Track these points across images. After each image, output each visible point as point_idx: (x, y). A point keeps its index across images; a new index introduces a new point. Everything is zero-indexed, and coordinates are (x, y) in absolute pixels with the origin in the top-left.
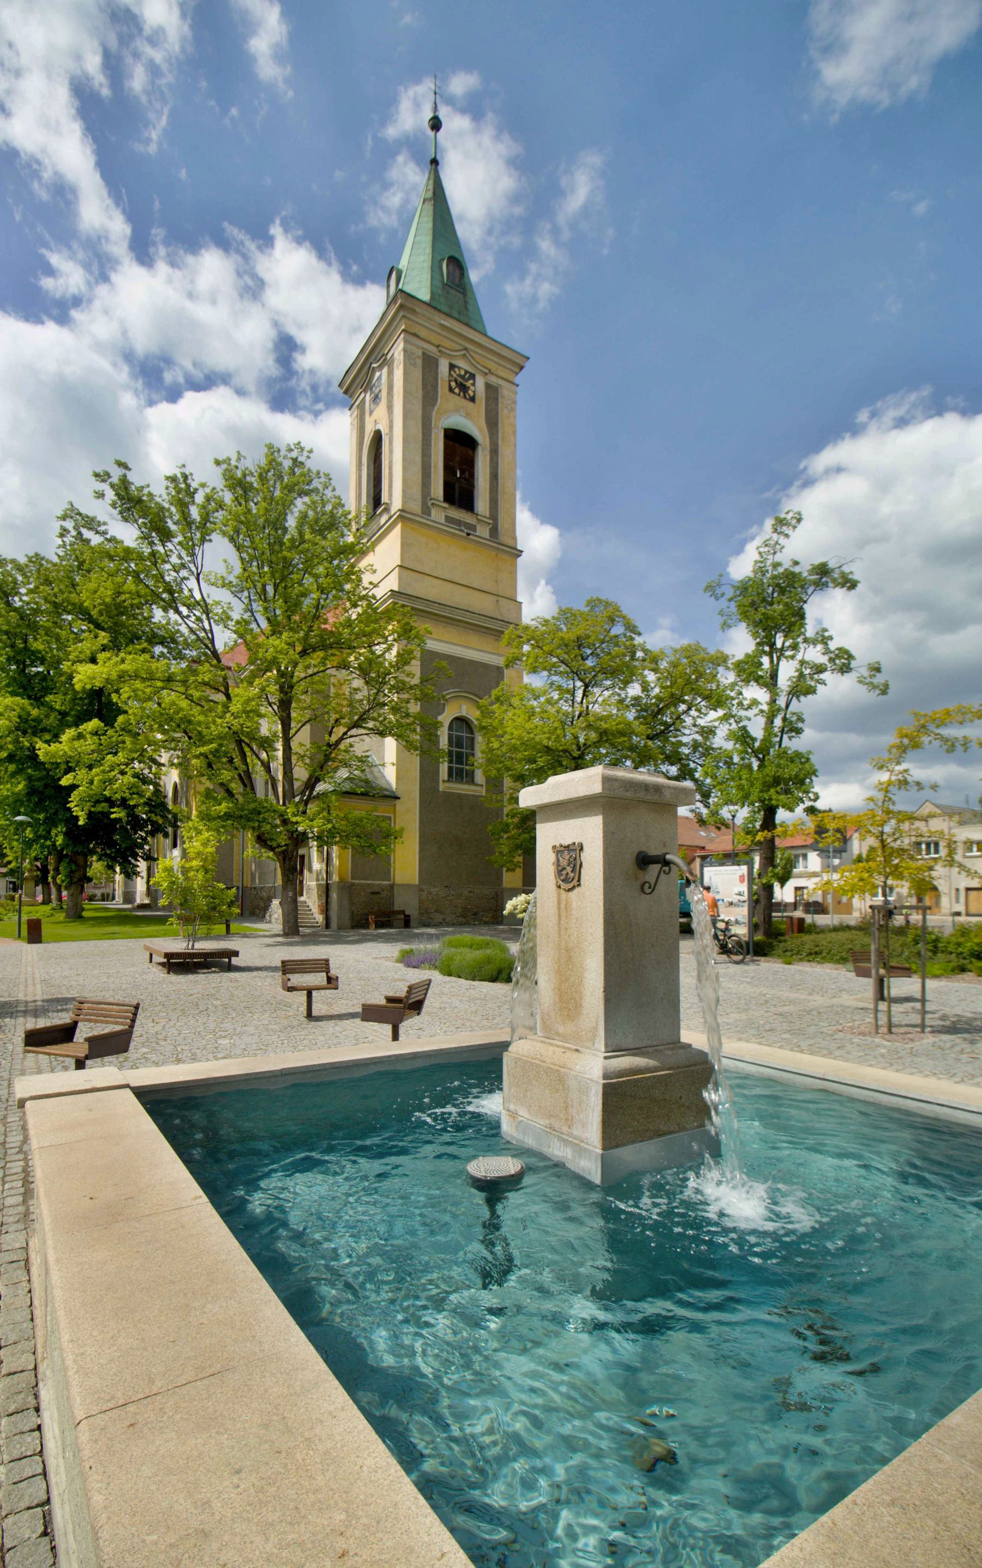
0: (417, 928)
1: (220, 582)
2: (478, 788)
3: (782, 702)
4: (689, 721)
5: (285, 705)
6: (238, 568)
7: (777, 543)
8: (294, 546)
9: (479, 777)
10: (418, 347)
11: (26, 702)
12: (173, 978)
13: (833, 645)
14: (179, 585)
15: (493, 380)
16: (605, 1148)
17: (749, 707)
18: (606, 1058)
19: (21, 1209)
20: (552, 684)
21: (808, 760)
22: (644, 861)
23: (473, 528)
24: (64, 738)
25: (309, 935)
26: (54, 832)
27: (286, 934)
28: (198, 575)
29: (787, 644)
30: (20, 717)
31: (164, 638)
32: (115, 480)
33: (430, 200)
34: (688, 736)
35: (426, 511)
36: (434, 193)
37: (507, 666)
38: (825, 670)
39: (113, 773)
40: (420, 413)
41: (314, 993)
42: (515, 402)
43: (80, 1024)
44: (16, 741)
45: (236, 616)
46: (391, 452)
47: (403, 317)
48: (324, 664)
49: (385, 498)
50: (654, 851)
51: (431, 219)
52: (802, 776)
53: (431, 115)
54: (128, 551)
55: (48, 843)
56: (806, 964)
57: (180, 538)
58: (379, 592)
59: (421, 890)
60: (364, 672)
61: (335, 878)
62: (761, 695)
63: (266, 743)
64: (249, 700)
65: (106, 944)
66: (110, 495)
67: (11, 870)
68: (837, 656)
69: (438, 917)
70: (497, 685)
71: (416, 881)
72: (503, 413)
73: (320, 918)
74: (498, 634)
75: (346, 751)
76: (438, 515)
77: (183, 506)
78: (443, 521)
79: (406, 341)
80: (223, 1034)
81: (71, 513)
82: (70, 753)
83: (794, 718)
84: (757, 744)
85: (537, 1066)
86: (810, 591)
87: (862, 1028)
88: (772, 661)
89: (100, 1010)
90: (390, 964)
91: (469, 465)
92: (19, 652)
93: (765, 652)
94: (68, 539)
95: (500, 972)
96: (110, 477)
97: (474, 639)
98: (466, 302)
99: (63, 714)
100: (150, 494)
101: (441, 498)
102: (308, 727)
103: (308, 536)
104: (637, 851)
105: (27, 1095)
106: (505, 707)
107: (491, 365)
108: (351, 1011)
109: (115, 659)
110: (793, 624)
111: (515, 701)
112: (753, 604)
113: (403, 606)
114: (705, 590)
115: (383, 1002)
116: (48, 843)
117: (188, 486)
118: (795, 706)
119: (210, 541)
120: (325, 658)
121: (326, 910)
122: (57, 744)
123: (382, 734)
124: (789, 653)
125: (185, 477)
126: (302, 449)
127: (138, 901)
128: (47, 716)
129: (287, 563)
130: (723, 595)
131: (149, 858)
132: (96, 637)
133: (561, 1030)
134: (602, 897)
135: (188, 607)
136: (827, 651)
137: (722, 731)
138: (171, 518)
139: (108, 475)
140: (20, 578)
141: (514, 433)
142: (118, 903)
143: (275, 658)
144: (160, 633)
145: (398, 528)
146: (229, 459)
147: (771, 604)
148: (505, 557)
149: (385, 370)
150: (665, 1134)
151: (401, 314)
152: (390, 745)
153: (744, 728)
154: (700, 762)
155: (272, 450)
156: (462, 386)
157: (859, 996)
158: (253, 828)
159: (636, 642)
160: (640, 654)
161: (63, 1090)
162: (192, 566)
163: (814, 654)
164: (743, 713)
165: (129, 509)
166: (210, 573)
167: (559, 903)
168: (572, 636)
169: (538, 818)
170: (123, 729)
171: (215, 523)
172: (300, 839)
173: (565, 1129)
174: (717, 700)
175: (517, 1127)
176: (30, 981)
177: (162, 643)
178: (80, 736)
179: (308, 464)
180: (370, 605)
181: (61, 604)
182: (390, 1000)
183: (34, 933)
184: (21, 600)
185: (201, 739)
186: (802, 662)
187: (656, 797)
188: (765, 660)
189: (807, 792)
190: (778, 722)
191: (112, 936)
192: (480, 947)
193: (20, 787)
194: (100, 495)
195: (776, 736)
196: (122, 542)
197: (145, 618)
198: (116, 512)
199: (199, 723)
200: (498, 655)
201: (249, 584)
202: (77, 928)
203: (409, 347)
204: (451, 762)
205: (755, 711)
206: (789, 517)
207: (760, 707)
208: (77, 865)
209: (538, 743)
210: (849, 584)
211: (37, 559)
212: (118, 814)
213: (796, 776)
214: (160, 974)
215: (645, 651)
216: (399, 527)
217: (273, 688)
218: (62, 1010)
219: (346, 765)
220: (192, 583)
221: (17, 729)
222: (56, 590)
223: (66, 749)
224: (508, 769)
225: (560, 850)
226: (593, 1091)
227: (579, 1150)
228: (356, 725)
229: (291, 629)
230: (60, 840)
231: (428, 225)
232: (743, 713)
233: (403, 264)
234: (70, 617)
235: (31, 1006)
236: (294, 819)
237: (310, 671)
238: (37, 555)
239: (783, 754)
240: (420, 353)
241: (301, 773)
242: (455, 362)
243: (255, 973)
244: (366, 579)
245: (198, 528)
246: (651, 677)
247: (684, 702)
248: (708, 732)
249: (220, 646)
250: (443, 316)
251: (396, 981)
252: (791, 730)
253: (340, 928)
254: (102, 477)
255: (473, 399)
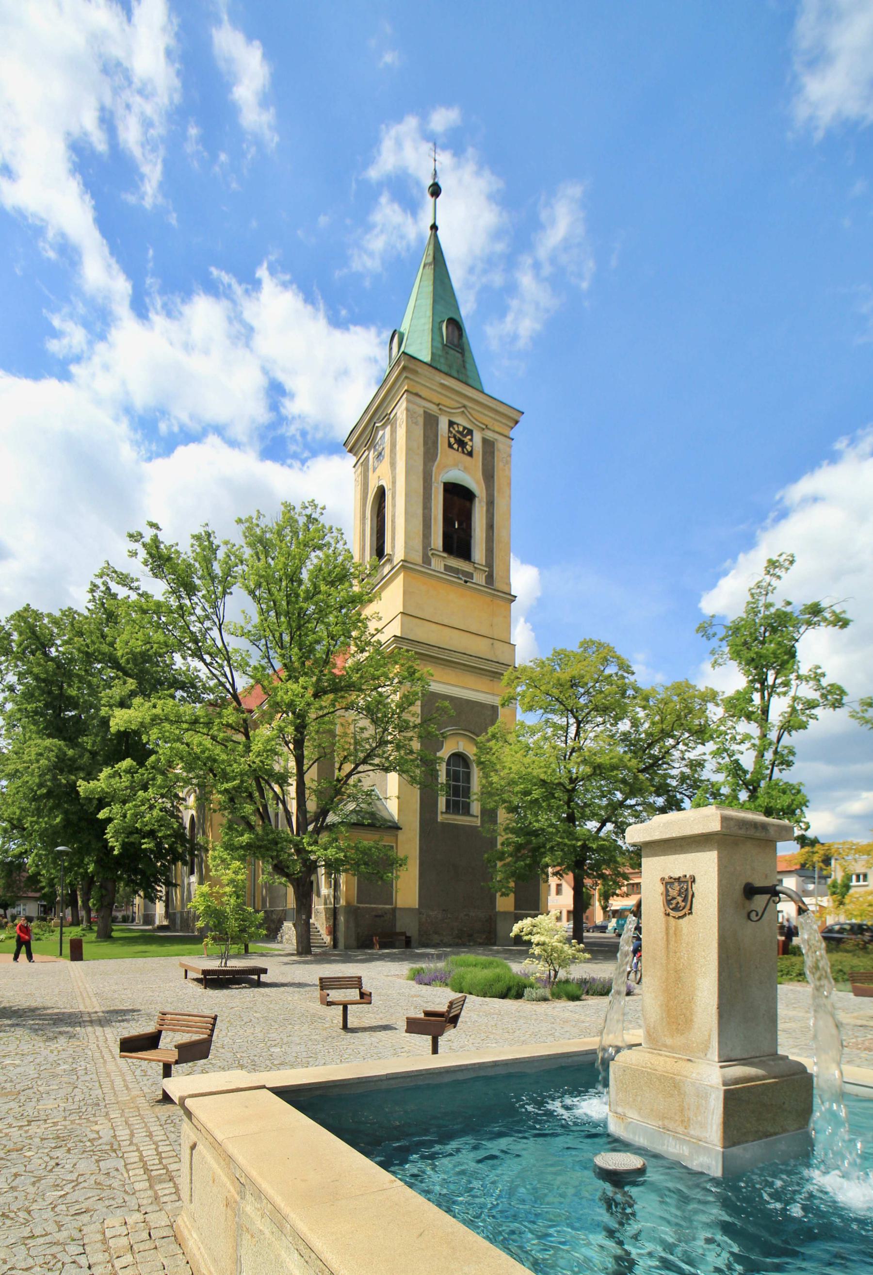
0: (417, 948)
1: (239, 632)
2: (474, 819)
3: (773, 735)
4: (676, 754)
5: (299, 744)
6: (256, 619)
7: (769, 585)
8: (308, 598)
9: (476, 808)
10: (420, 406)
11: (62, 743)
12: (210, 992)
13: (824, 682)
14: (204, 635)
15: (490, 435)
16: (724, 1147)
17: (742, 742)
18: (721, 1067)
19: (150, 1193)
20: (547, 721)
21: (799, 792)
22: (750, 891)
23: (470, 575)
24: (102, 776)
25: (320, 954)
26: (86, 860)
27: (299, 953)
28: (220, 625)
29: (778, 681)
30: (57, 757)
31: (184, 683)
32: (147, 539)
33: (430, 264)
34: (677, 769)
35: (427, 561)
36: (434, 258)
37: (503, 705)
38: (818, 706)
39: (143, 808)
40: (421, 468)
41: (349, 1006)
42: (510, 456)
43: (164, 1033)
44: (54, 778)
45: (253, 662)
46: (394, 506)
47: (406, 378)
48: (334, 706)
49: (388, 550)
50: (759, 883)
51: (431, 282)
52: (794, 806)
53: (431, 182)
54: (158, 605)
55: (81, 870)
56: (796, 983)
57: (204, 592)
58: (383, 638)
59: (420, 913)
60: (370, 711)
61: (342, 902)
62: (752, 729)
63: (282, 780)
64: (269, 740)
65: (140, 961)
66: (143, 554)
67: (45, 894)
68: (829, 692)
69: (436, 939)
70: (493, 723)
71: (417, 907)
72: (499, 465)
73: (328, 939)
74: (496, 675)
75: (355, 786)
76: (438, 564)
77: (207, 562)
78: (442, 570)
79: (408, 401)
80: (273, 1043)
81: (108, 571)
82: (106, 789)
83: (786, 752)
84: (748, 776)
85: (648, 1073)
86: (801, 630)
87: (867, 1044)
88: (763, 697)
89: (180, 1021)
90: (402, 981)
91: (466, 517)
92: (56, 698)
93: (756, 690)
94: (98, 594)
95: (509, 989)
96: (142, 537)
97: (470, 680)
98: (464, 361)
99: (94, 754)
100: (177, 552)
101: (441, 549)
102: (316, 764)
103: (323, 588)
104: (744, 882)
105: (186, 1094)
106: (500, 744)
107: (487, 420)
108: (380, 1024)
109: (147, 705)
110: (787, 662)
111: (511, 738)
112: (745, 643)
113: (408, 651)
114: (697, 631)
115: (422, 1016)
116: (81, 870)
117: (211, 543)
118: (786, 740)
119: (231, 593)
120: (335, 700)
121: (333, 931)
122: (95, 782)
123: (387, 770)
124: (781, 690)
125: (209, 535)
126: (316, 506)
127: (157, 923)
128: (81, 756)
129: (301, 612)
130: (714, 635)
131: (168, 884)
132: (125, 683)
133: (669, 1041)
134: (716, 924)
135: (210, 654)
136: (819, 688)
137: (711, 765)
138: (196, 574)
139: (141, 535)
140: (56, 630)
141: (509, 484)
142: (138, 926)
143: (293, 701)
144: (183, 678)
145: (401, 577)
146: (251, 518)
147: (763, 643)
148: (502, 603)
149: (388, 429)
150: (771, 1135)
151: (404, 375)
152: (393, 778)
153: (737, 762)
154: (687, 793)
155: (289, 508)
156: (460, 442)
157: (855, 1014)
158: (272, 858)
159: (627, 681)
160: (630, 692)
161: (214, 1090)
162: (214, 617)
163: (807, 691)
164: (735, 747)
165: (159, 566)
166: (230, 623)
167: (667, 929)
168: (565, 677)
169: (643, 854)
170: (153, 768)
171: (235, 577)
172: (311, 867)
173: (680, 1129)
174: (702, 734)
175: (626, 1128)
176: (85, 995)
177: (182, 688)
178: (117, 774)
179: (322, 520)
180: (377, 651)
181: (93, 654)
182: (427, 1014)
183: (76, 953)
184: (57, 651)
185: (225, 777)
186: (795, 699)
187: (763, 834)
188: (756, 697)
189: (798, 822)
190: (769, 755)
191: (144, 954)
192: (485, 966)
193: (58, 820)
194: (134, 554)
195: (768, 769)
196: (152, 596)
197: (167, 666)
198: (148, 569)
199: (223, 761)
200: (493, 694)
201: (268, 633)
202: (106, 947)
203: (411, 406)
204: (447, 793)
205: (747, 745)
206: (781, 559)
207: (753, 741)
208: (106, 889)
209: (534, 777)
210: (842, 622)
211: (70, 613)
212: (147, 844)
213: (789, 806)
214: (199, 989)
215: (637, 690)
216: (401, 576)
217: (291, 729)
218: (123, 1021)
219: (355, 799)
220: (215, 633)
221: (55, 767)
222: (88, 641)
223: (103, 786)
224: (504, 801)
225: (668, 883)
226: (713, 1096)
227: (698, 1145)
228: (364, 762)
229: (306, 674)
230: (91, 868)
231: (429, 288)
232: (735, 747)
233: (405, 327)
234: (99, 666)
235: (94, 1017)
236: (310, 849)
237: (321, 713)
238: (70, 609)
239: (773, 785)
240: (421, 411)
241: (312, 805)
242: (456, 419)
243: (282, 989)
244: (372, 626)
245: (220, 582)
246: (641, 714)
247: (673, 737)
248: (697, 765)
249: (240, 689)
250: (442, 375)
251: (412, 997)
252: (782, 763)
253: (347, 947)
254: (135, 537)
255: (470, 454)
